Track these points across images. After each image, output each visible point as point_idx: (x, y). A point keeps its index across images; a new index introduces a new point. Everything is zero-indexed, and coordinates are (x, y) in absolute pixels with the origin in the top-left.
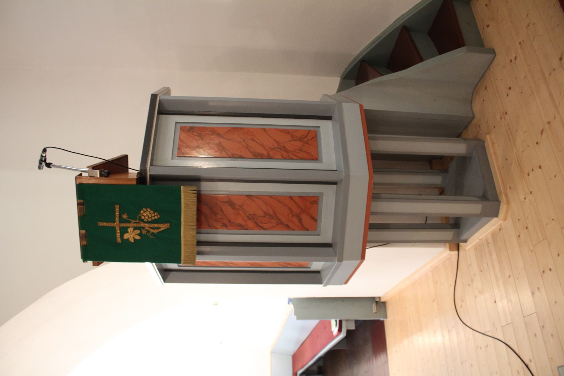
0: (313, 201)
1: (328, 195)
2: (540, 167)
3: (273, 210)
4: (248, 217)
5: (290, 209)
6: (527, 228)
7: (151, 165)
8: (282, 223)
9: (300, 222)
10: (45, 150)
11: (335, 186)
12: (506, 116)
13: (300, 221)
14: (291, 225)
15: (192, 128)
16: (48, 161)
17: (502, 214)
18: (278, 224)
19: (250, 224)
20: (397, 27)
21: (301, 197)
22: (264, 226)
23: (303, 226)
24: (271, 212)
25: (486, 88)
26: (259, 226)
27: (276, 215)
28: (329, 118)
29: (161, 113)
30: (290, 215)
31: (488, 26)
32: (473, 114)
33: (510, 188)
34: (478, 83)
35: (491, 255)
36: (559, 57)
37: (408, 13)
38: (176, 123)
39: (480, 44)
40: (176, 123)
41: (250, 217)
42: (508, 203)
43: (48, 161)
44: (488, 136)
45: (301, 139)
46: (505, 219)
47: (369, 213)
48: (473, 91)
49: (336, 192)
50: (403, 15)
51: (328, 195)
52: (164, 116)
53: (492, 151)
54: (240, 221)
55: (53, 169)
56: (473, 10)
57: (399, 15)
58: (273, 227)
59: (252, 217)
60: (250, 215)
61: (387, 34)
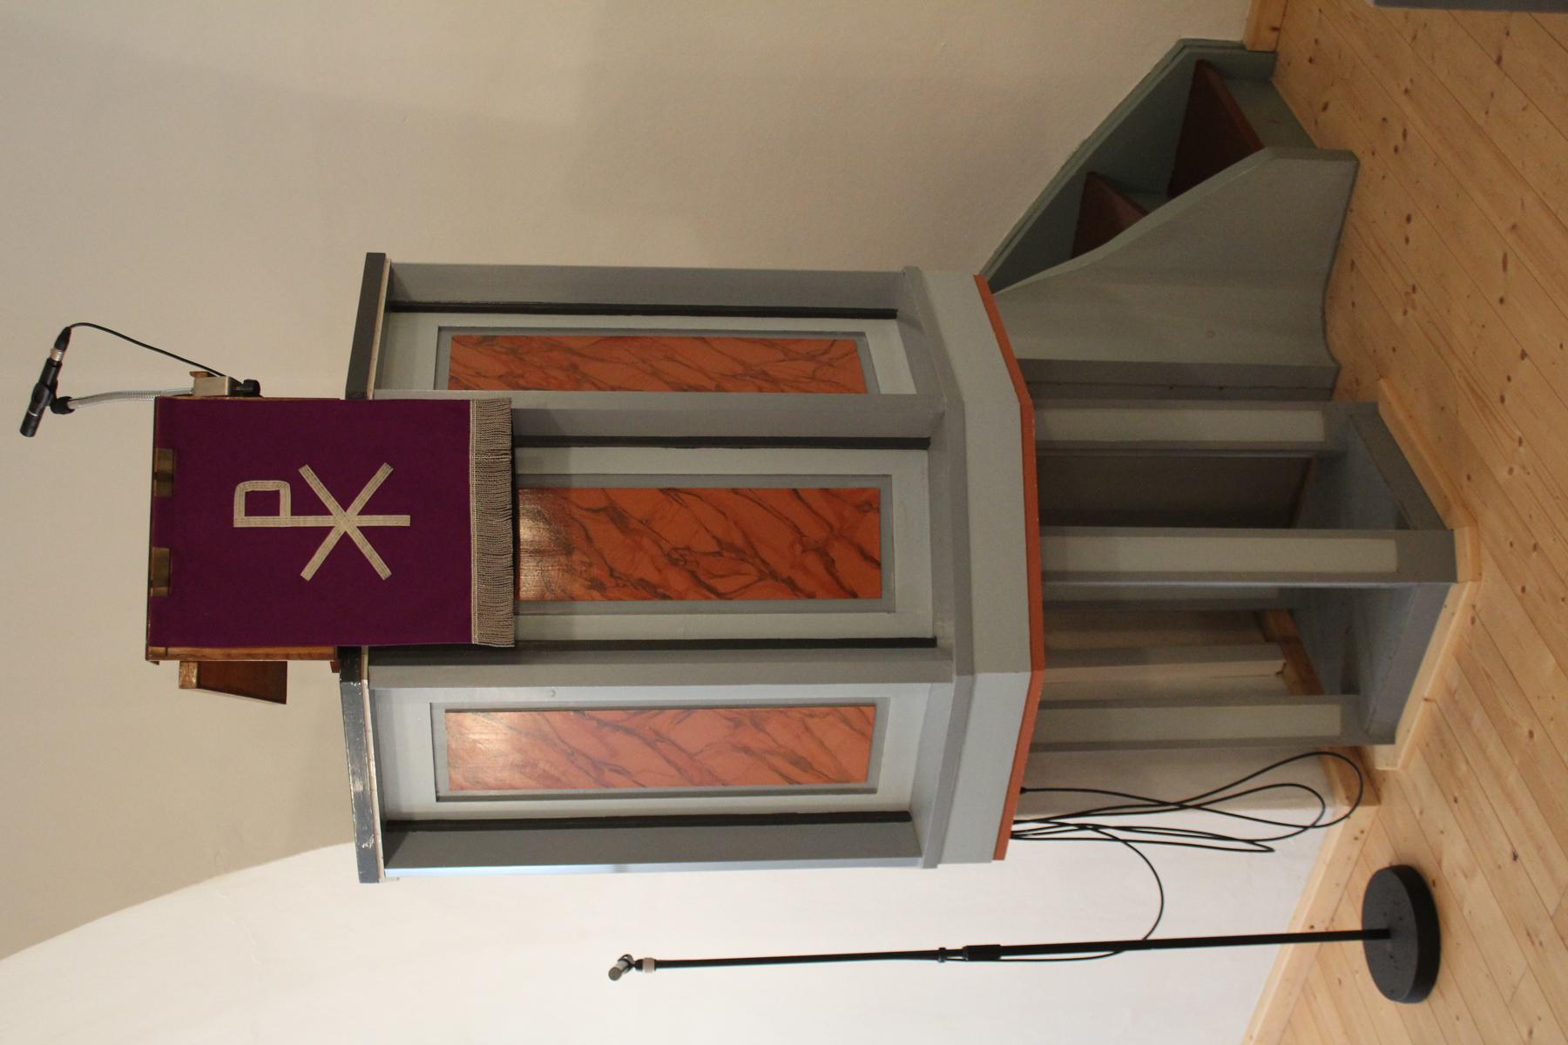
0: (866, 503)
1: (906, 481)
2: (1524, 355)
3: (745, 536)
4: (668, 556)
5: (796, 529)
6: (1535, 547)
7: (377, 386)
8: (774, 575)
9: (827, 569)
10: (63, 340)
11: (923, 454)
12: (1414, 296)
13: (829, 565)
14: (800, 579)
15: (486, 339)
16: (60, 394)
17: (1464, 566)
18: (760, 580)
19: (677, 580)
20: (1073, 178)
21: (825, 491)
22: (720, 585)
23: (842, 587)
24: (738, 540)
25: (1353, 263)
26: (707, 588)
27: (753, 548)
28: (889, 314)
29: (395, 307)
30: (798, 548)
31: (1325, 108)
32: (1333, 359)
33: (1469, 478)
34: (1327, 259)
35: (1467, 721)
36: (1495, 57)
37: (1098, 132)
38: (440, 329)
39: (1300, 142)
40: (440, 329)
41: (675, 556)
42: (1474, 520)
43: (60, 394)
44: (1382, 383)
45: (811, 357)
46: (1478, 576)
47: (1042, 576)
48: (1324, 295)
49: (930, 469)
50: (1084, 143)
51: (906, 481)
52: (404, 316)
53: (1401, 416)
54: (647, 572)
55: (80, 410)
56: (1281, 91)
57: (1073, 145)
58: (747, 587)
59: (680, 558)
60: (676, 549)
61: (1042, 209)
